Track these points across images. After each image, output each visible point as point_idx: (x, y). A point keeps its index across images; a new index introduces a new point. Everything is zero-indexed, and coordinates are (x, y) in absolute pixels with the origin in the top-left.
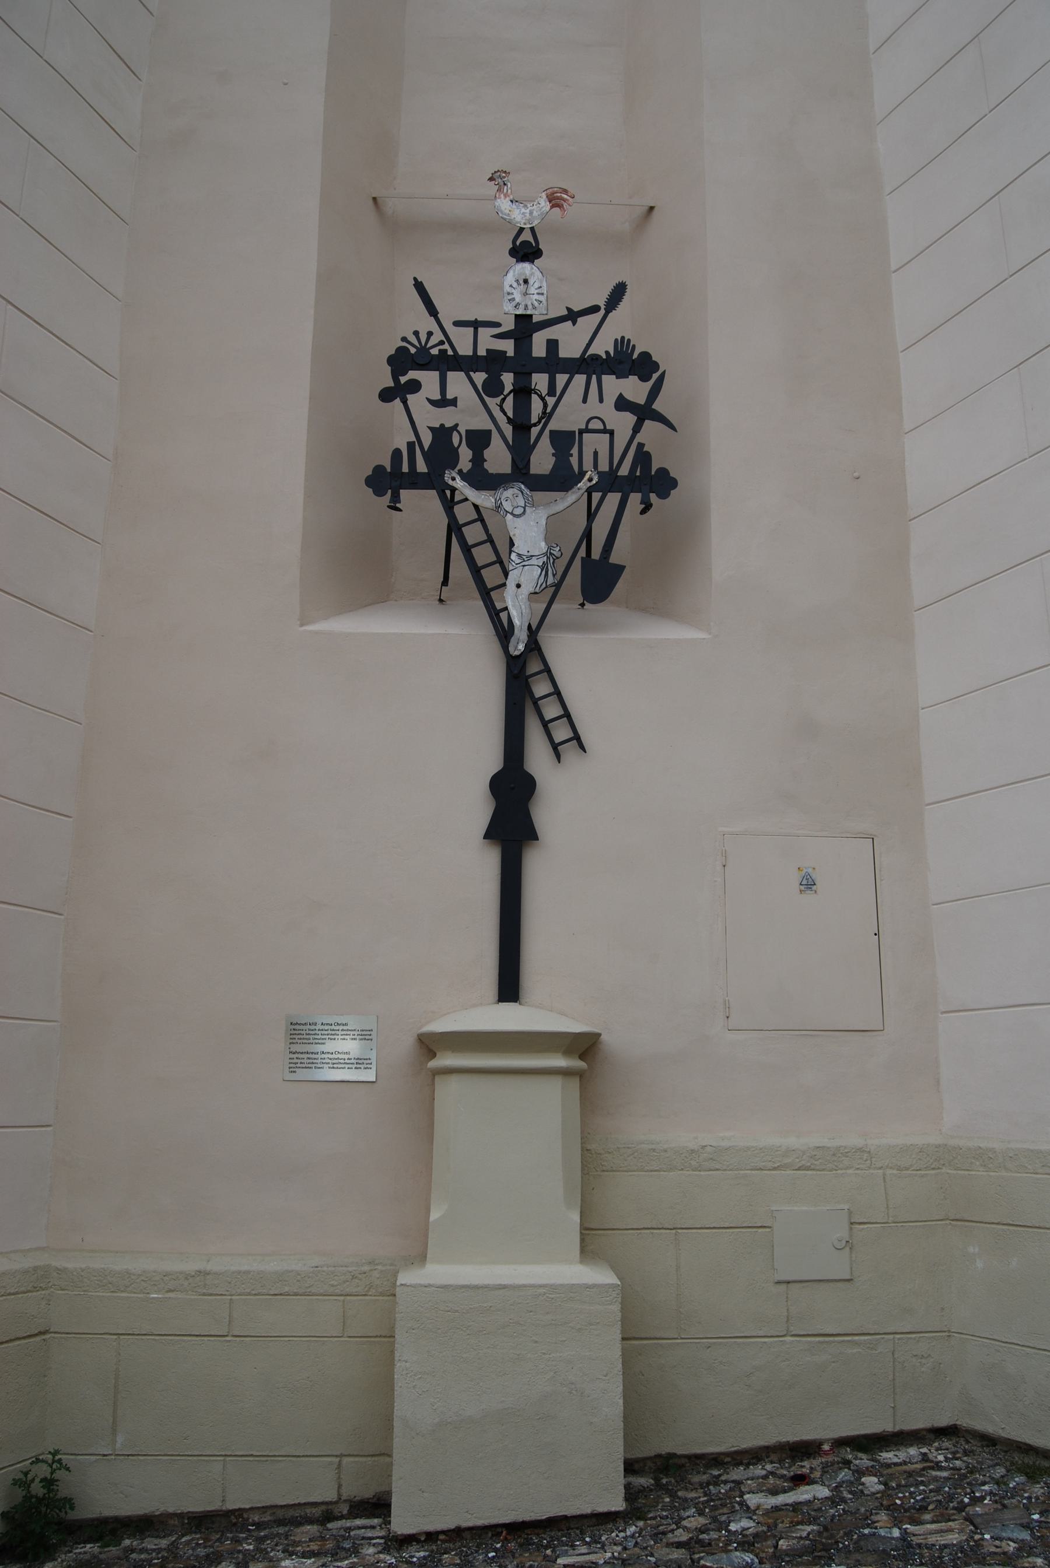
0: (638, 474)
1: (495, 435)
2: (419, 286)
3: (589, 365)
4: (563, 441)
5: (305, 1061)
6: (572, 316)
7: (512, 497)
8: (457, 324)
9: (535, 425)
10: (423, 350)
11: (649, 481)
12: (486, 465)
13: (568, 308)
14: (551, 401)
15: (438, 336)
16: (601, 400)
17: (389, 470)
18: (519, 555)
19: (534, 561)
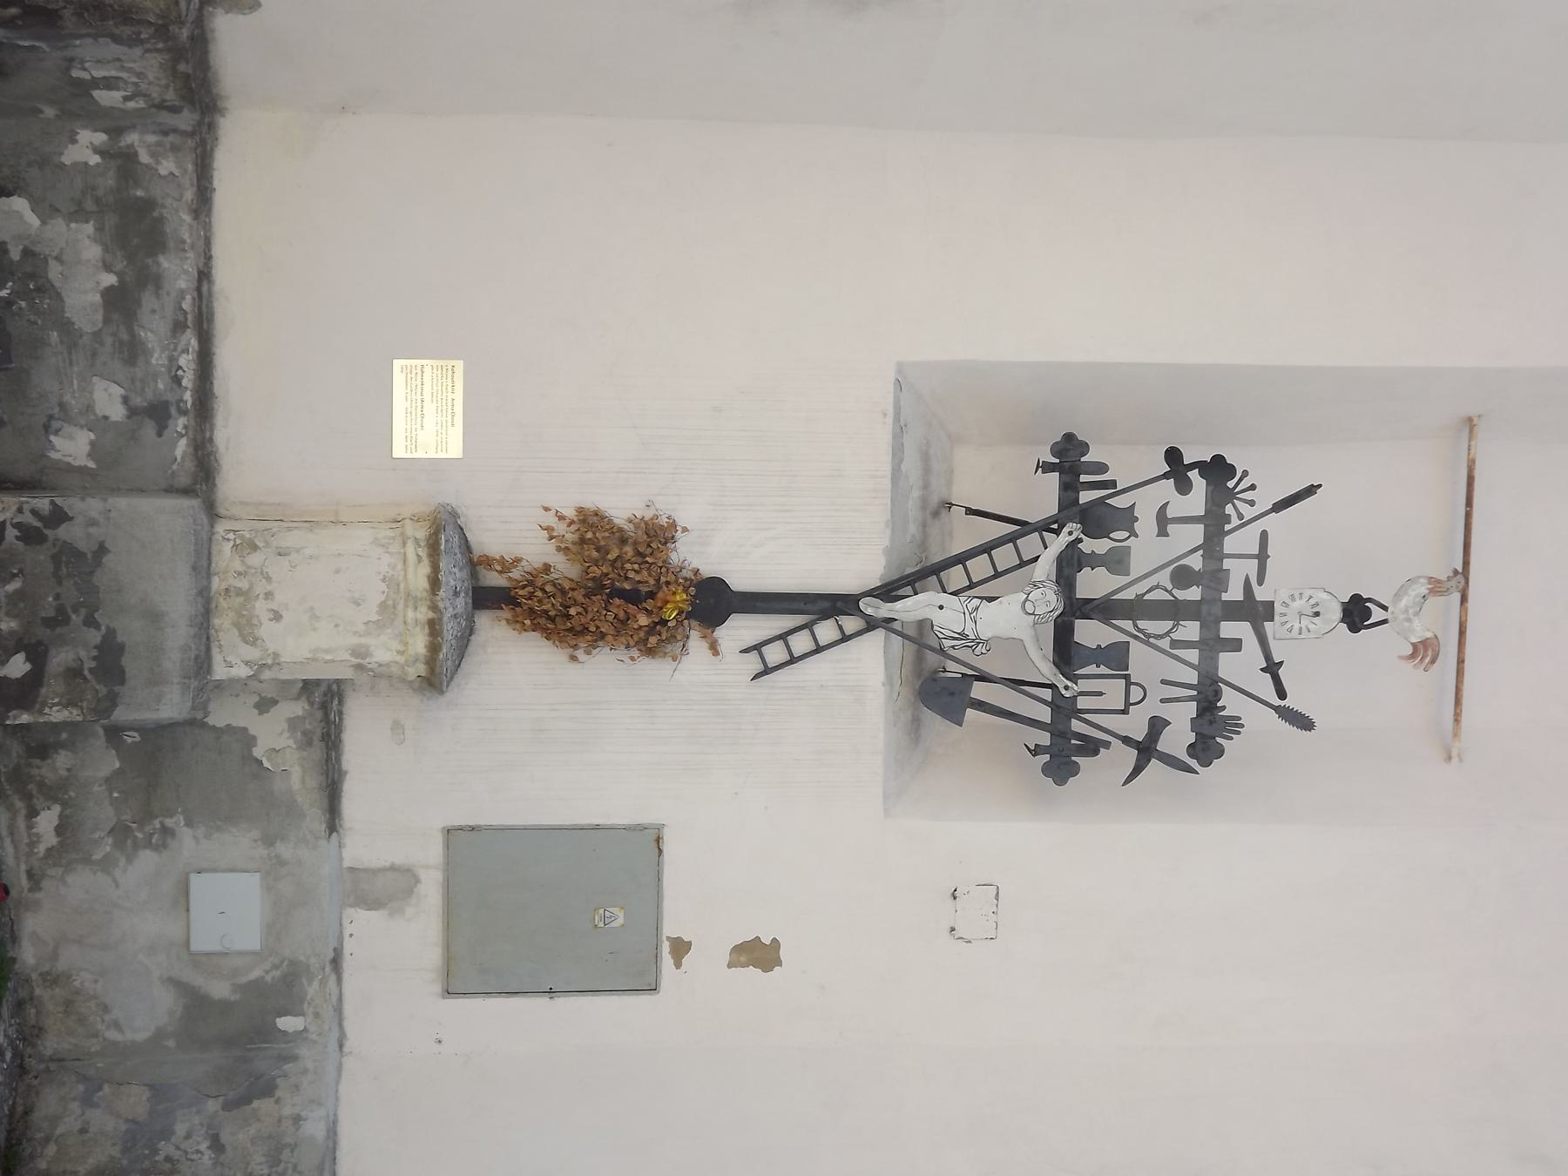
2: (1311, 490)
4: (1115, 658)
7: (1048, 601)
8: (1264, 536)
9: (1135, 626)
10: (1231, 496)
11: (1064, 750)
14: (1164, 643)
15: (1248, 512)
19: (970, 624)
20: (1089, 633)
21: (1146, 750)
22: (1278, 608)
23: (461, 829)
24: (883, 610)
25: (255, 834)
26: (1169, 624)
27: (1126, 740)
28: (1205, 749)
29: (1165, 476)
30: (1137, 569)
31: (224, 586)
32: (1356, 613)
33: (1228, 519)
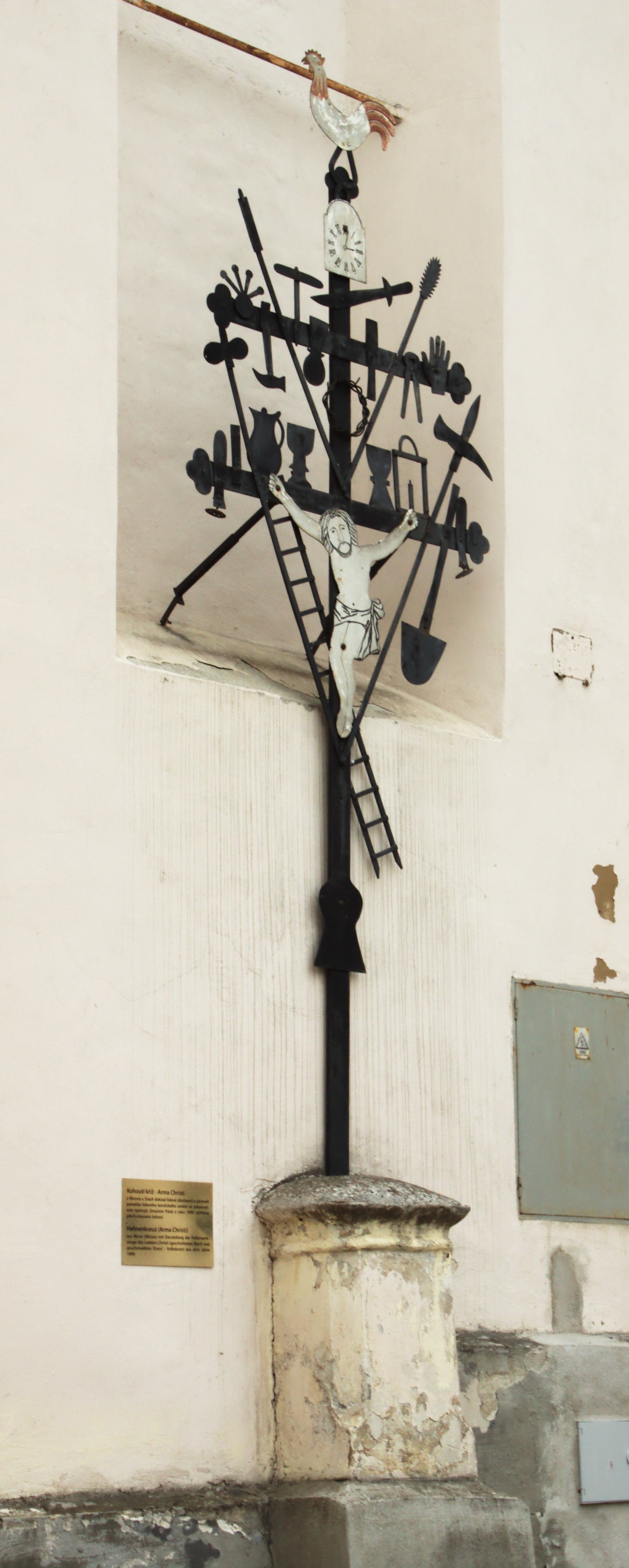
0: (454, 526)
1: (317, 435)
2: (244, 203)
3: (408, 367)
4: (384, 461)
5: (142, 1240)
6: (389, 292)
7: (338, 525)
8: (280, 269)
9: (355, 435)
10: (244, 297)
11: (460, 536)
12: (307, 474)
13: (385, 281)
14: (371, 405)
15: (258, 281)
16: (420, 420)
17: (211, 458)
18: (345, 607)
19: (358, 618)
20: (361, 488)
21: (462, 448)
22: (340, 271)
23: (520, 1204)
24: (346, 712)
25: (547, 1429)
26: (354, 396)
27: (454, 467)
28: (455, 383)
29: (230, 367)
30: (311, 424)
31: (400, 1464)
32: (341, 185)
33: (265, 305)
